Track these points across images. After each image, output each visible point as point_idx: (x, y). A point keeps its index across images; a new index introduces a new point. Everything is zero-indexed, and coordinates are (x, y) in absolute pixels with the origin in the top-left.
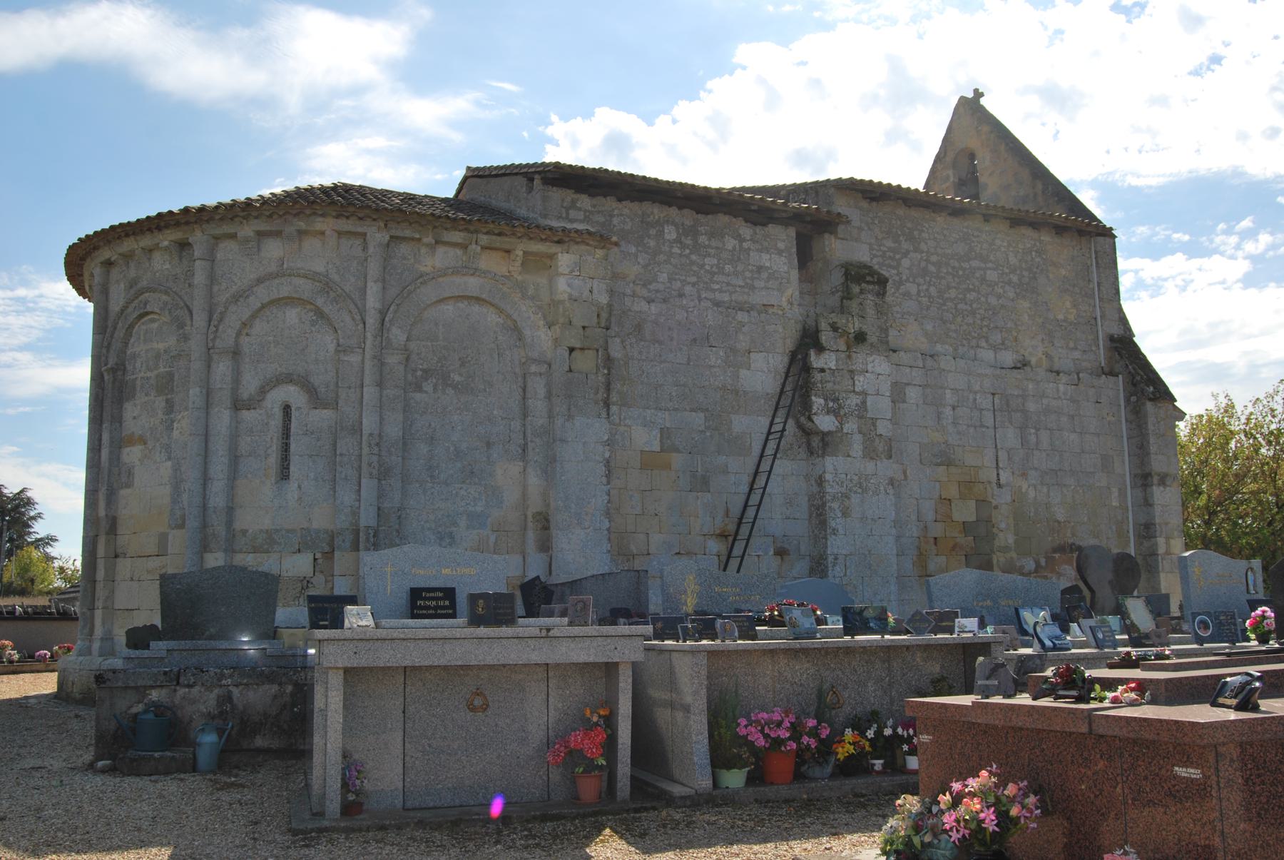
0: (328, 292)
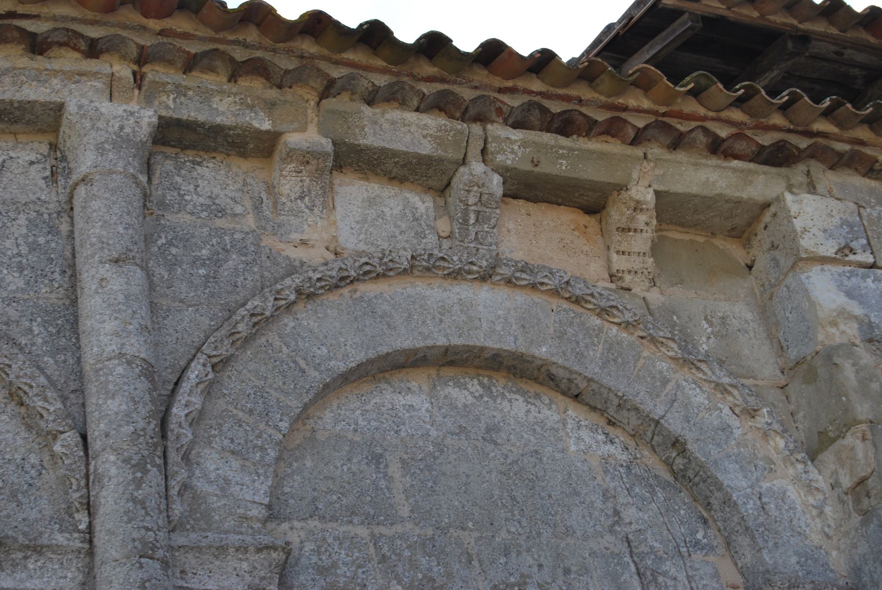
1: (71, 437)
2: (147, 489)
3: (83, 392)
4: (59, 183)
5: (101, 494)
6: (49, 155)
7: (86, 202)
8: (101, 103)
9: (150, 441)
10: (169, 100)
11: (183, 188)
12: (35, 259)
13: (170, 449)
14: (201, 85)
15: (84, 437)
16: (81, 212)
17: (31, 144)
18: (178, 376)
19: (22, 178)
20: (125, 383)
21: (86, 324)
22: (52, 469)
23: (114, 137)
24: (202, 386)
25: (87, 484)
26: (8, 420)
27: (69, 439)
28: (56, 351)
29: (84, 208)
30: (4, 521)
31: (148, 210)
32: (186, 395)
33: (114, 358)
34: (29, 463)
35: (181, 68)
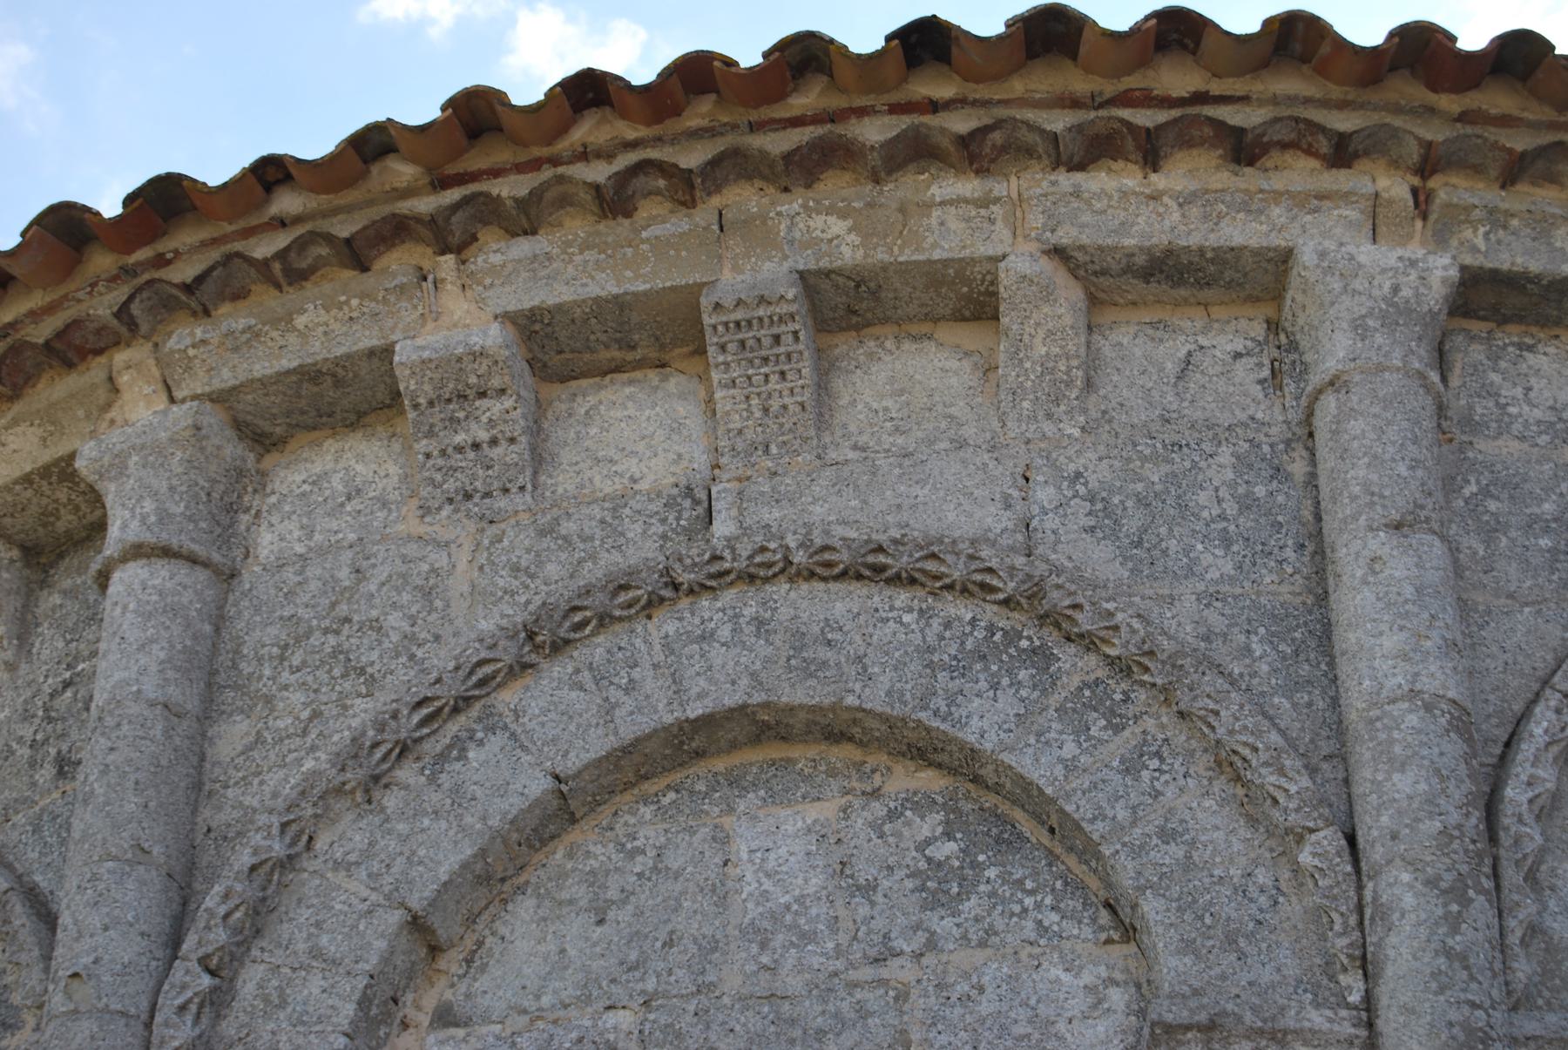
0: (1041, 657)
1: (1329, 839)
2: (1470, 934)
3: (1344, 760)
4: (1286, 390)
5: (1387, 941)
6: (1267, 342)
7: (1338, 422)
8: (1358, 247)
9: (1471, 847)
10: (1476, 237)
11: (1503, 392)
12: (1250, 524)
13: (1504, 863)
14: (1533, 208)
15: (1351, 839)
16: (1331, 439)
17: (1234, 322)
18: (1510, 730)
19: (1221, 383)
20: (1422, 744)
21: (1347, 638)
22: (1296, 894)
23: (1384, 307)
24: (1555, 749)
25: (1361, 923)
26: (1215, 807)
27: (1326, 843)
28: (1293, 687)
29: (1335, 432)
30: (1216, 986)
31: (1444, 433)
32: (1528, 765)
33: (1402, 698)
34: (1254, 883)
35: (1497, 179)
